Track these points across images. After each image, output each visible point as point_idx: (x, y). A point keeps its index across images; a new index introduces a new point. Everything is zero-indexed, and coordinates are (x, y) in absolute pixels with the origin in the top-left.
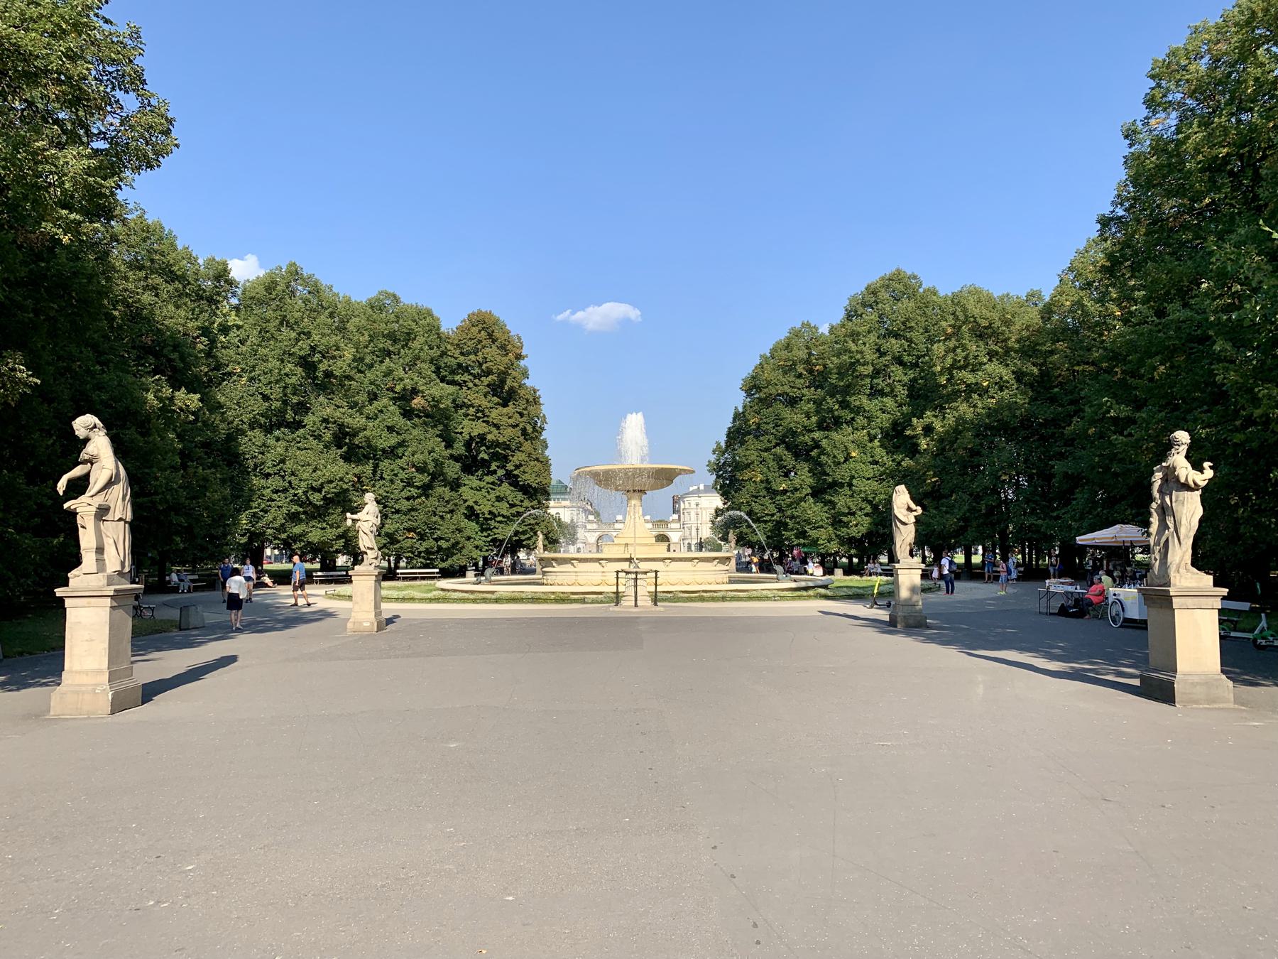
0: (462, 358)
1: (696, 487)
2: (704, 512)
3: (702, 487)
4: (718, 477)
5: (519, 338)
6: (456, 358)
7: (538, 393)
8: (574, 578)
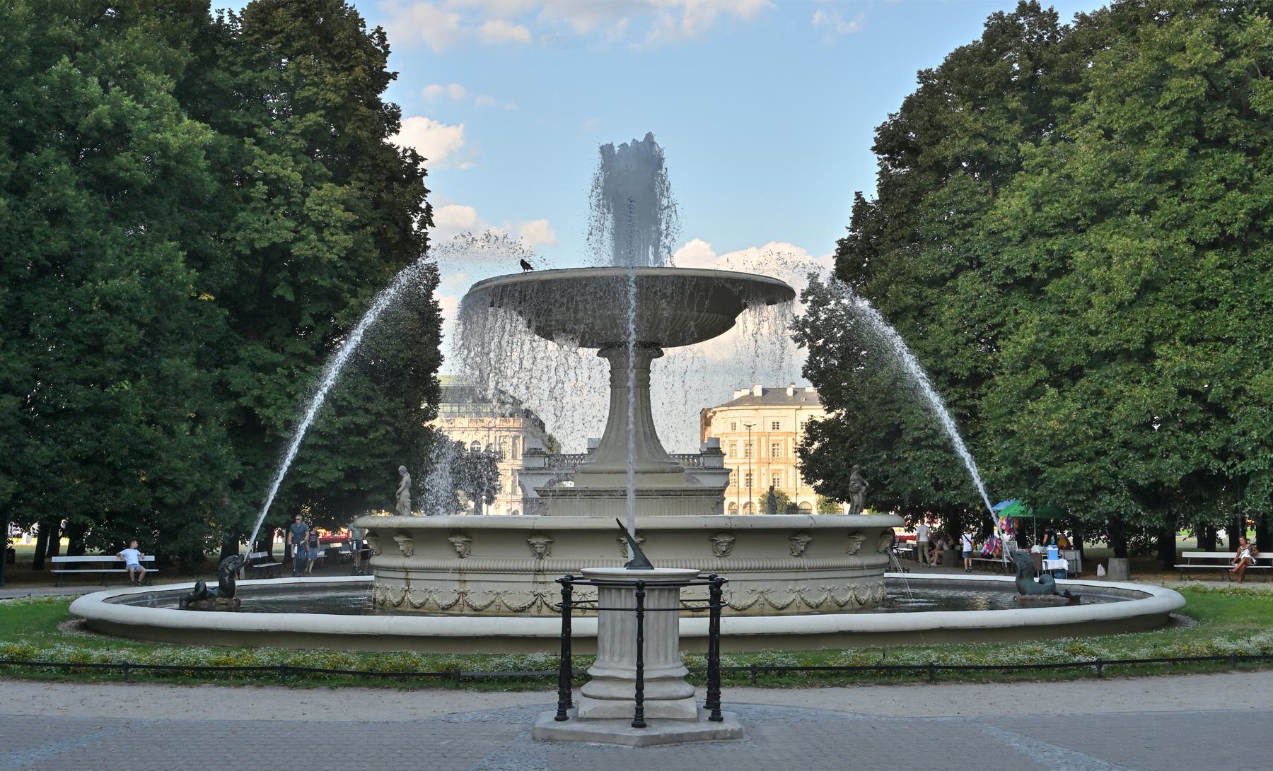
0: (249, 74)
1: (746, 392)
2: (763, 440)
3: (758, 392)
4: (815, 351)
5: (382, 37)
6: (235, 74)
7: (421, 166)
8: (457, 586)
